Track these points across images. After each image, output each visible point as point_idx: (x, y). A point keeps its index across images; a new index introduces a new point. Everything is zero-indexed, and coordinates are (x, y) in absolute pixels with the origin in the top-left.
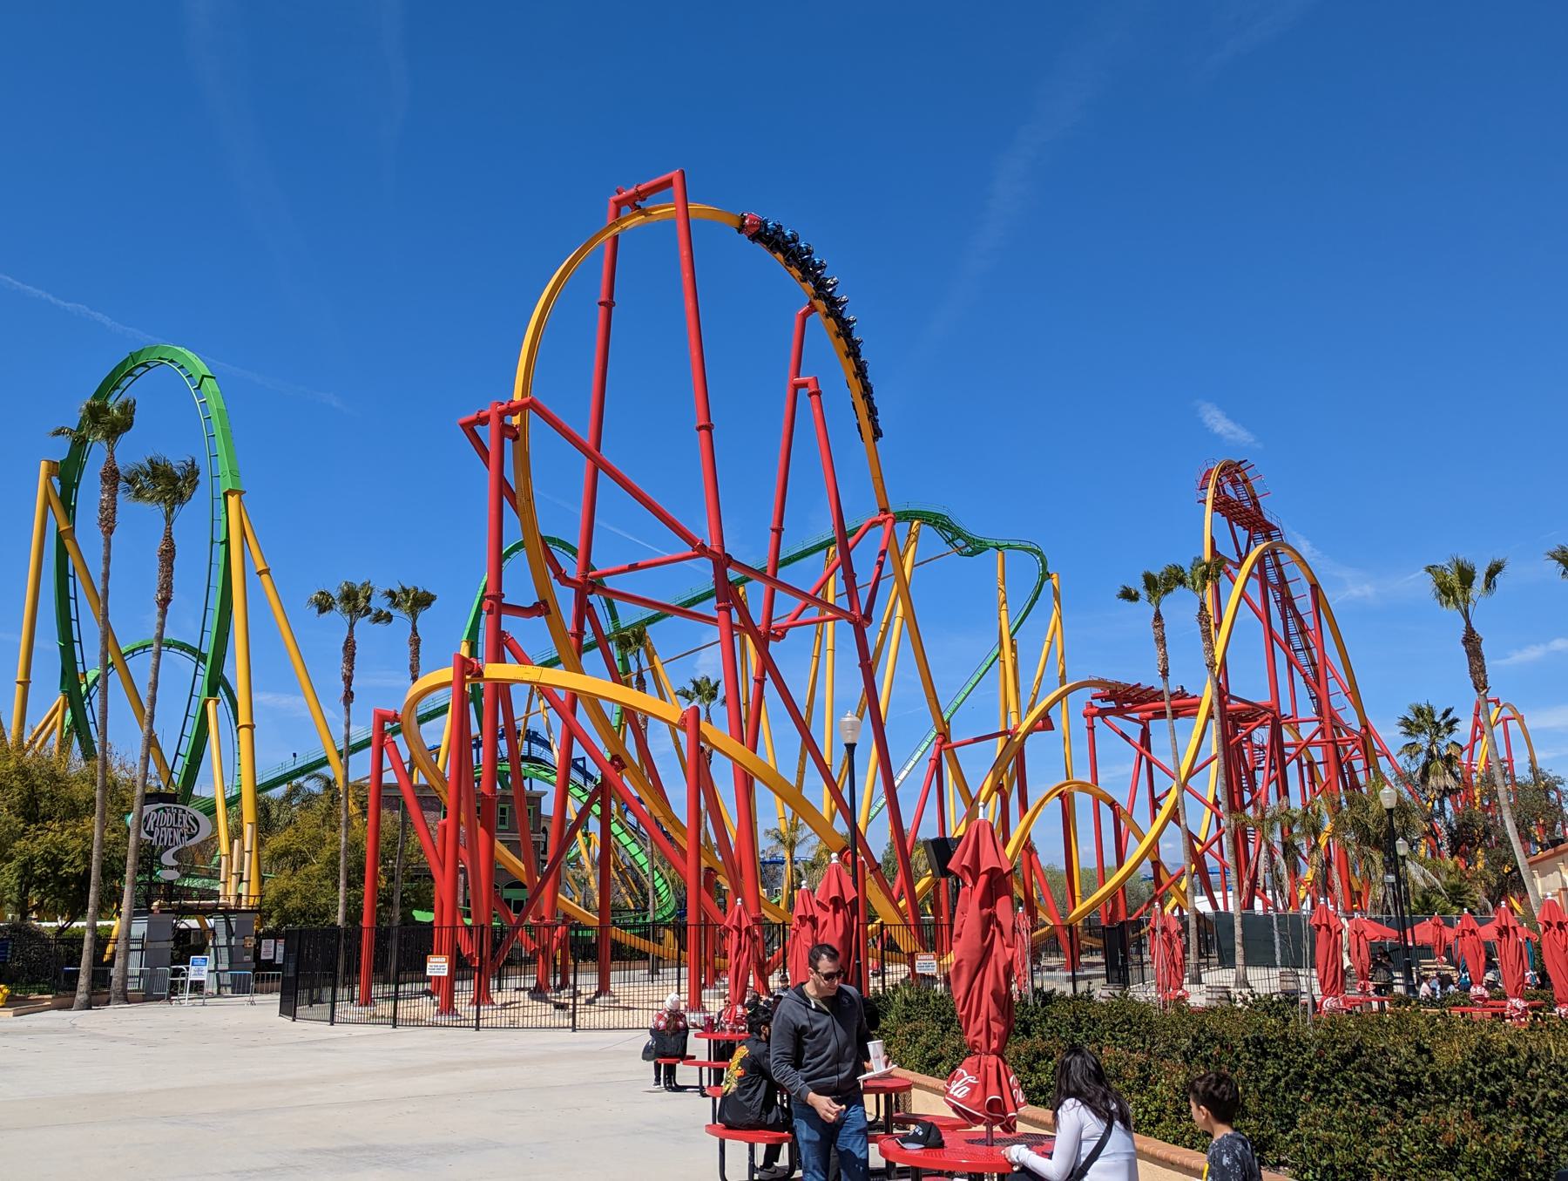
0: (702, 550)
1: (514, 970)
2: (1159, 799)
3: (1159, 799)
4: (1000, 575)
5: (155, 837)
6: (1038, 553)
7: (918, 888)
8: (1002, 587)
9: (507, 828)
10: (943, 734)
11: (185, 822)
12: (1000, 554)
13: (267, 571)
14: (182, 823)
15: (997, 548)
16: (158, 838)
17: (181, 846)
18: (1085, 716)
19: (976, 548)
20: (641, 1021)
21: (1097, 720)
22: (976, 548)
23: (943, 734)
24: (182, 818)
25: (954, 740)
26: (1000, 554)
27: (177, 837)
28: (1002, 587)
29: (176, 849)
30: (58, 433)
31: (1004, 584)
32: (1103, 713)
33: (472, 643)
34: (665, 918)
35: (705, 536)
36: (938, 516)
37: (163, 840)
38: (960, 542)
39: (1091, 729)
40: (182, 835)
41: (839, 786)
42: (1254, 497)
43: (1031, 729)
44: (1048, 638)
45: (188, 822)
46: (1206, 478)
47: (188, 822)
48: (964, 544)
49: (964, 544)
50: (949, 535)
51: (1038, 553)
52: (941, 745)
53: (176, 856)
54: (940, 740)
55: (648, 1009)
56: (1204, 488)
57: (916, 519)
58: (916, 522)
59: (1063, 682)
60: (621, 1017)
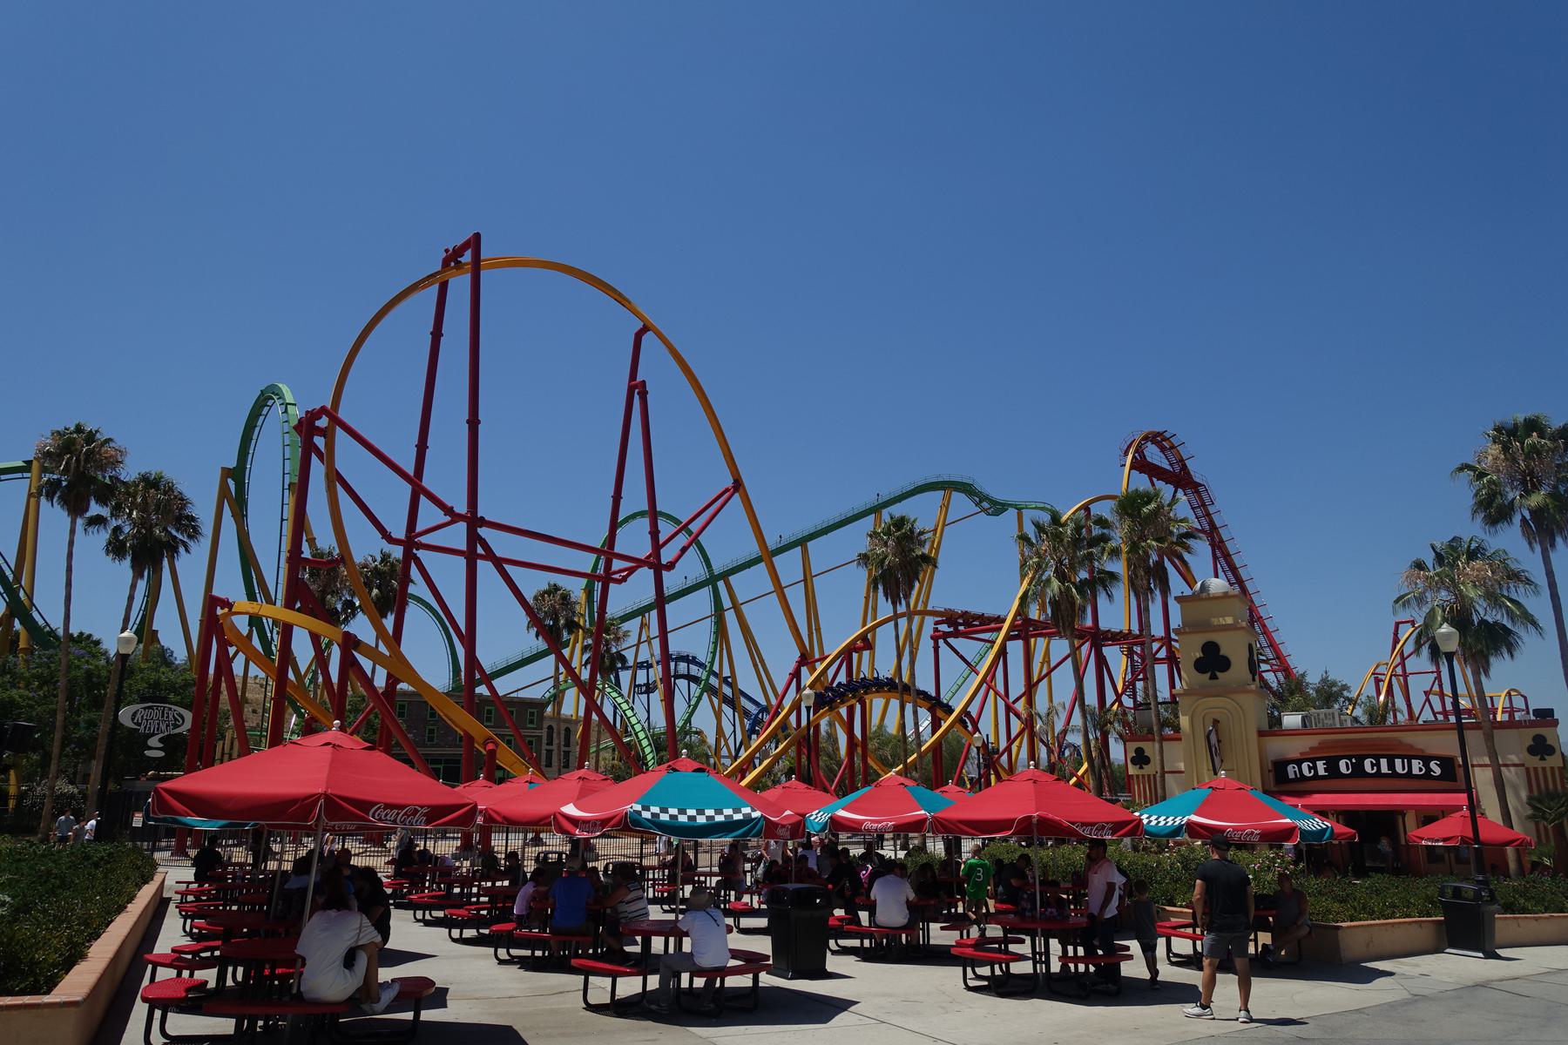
0: (455, 517)
5: (142, 727)
7: (909, 761)
9: (492, 724)
11: (171, 716)
14: (168, 717)
16: (145, 727)
17: (166, 734)
20: (444, 845)
24: (168, 713)
27: (163, 727)
29: (161, 735)
30: (1461, 469)
33: (590, 591)
35: (461, 508)
37: (150, 728)
40: (168, 726)
41: (599, 702)
42: (1182, 460)
44: (4, 595)
45: (173, 716)
46: (1129, 447)
47: (173, 716)
53: (161, 740)
56: (1126, 453)
59: (864, 625)
60: (444, 845)
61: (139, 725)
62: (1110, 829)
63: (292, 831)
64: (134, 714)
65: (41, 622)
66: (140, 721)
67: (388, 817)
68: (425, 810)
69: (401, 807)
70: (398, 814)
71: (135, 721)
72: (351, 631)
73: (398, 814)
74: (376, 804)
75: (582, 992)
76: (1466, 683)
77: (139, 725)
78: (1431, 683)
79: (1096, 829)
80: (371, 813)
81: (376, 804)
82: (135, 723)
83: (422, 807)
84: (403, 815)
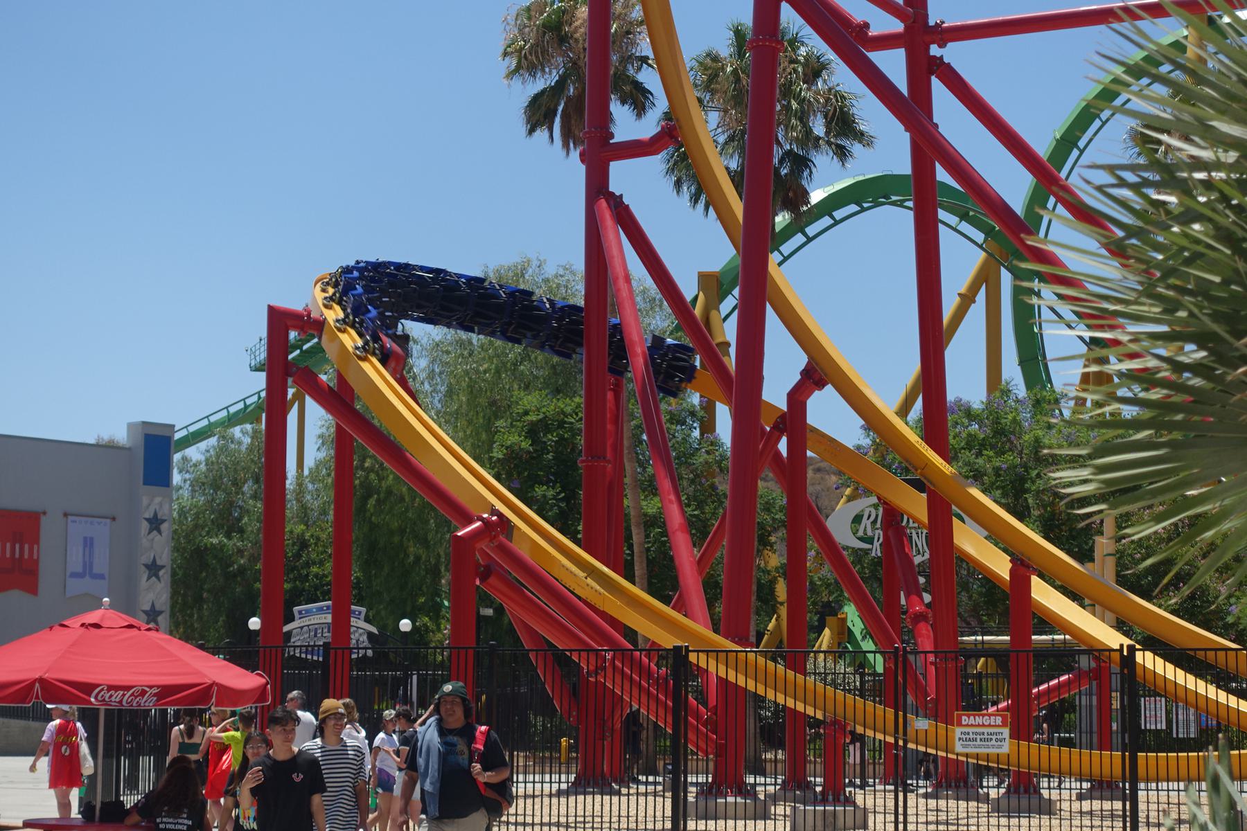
61: (870, 540)
62: (155, 695)
63: (254, 705)
64: (857, 519)
65: (1178, 18)
66: (869, 533)
67: (113, 699)
68: (155, 691)
69: (128, 688)
70: (124, 695)
71: (860, 533)
72: (659, 156)
73: (124, 695)
74: (98, 685)
75: (908, 813)
76: (1090, 195)
77: (870, 540)
78: (253, 393)
79: (132, 694)
80: (94, 694)
81: (98, 685)
82: (861, 539)
83: (151, 687)
84: (131, 696)
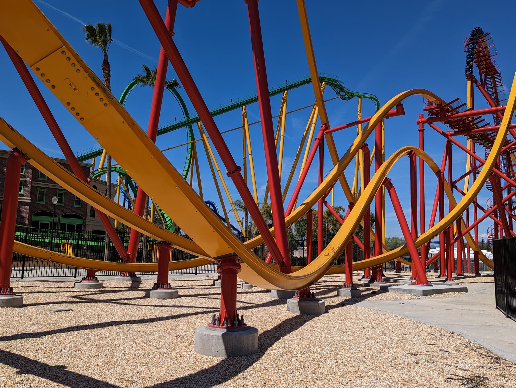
1: (16, 263)
2: (456, 182)
3: (456, 182)
4: (359, 109)
6: (376, 100)
8: (360, 114)
10: (326, 124)
12: (360, 99)
13: (219, 170)
15: (359, 97)
18: (418, 123)
19: (350, 96)
21: (426, 126)
22: (350, 96)
23: (326, 124)
25: (332, 127)
26: (360, 99)
28: (360, 114)
31: (361, 112)
32: (430, 121)
34: (490, 240)
36: (334, 81)
38: (342, 93)
39: (422, 131)
43: (386, 115)
48: (344, 94)
49: (344, 94)
50: (338, 90)
51: (376, 100)
52: (324, 130)
54: (323, 128)
55: (210, 271)
57: (324, 81)
58: (324, 83)
